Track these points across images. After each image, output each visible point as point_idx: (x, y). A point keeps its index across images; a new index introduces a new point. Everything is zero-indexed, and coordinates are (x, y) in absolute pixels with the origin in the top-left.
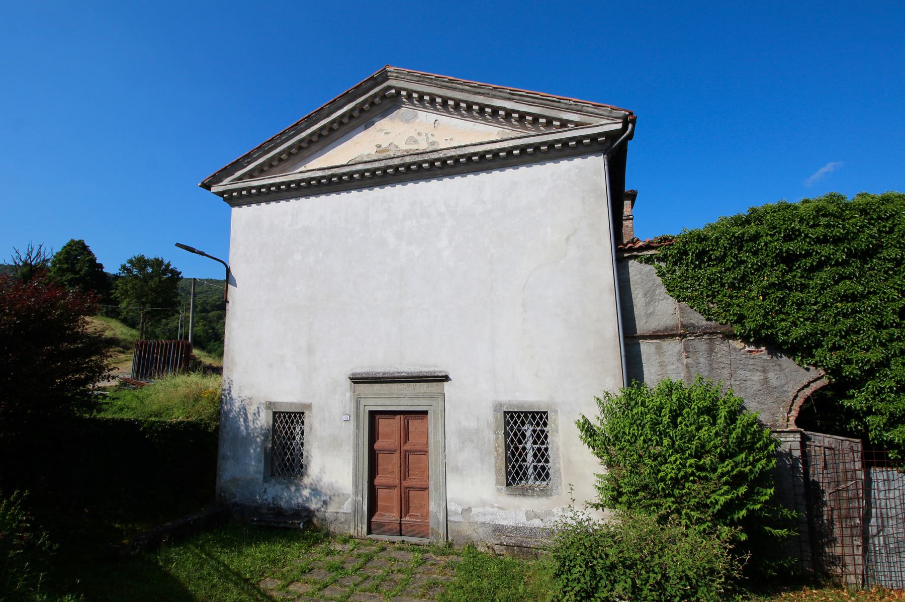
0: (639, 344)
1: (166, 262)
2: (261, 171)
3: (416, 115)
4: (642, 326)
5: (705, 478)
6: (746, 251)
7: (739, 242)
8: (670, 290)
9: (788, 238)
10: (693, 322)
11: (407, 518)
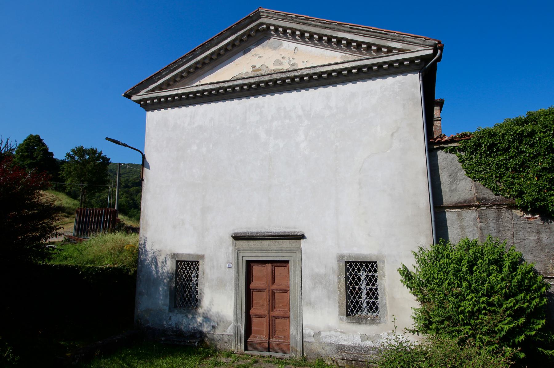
0: (445, 212)
1: (99, 151)
2: (167, 85)
4: (447, 199)
5: (494, 311)
7: (519, 137)
10: (485, 196)
11: (274, 339)
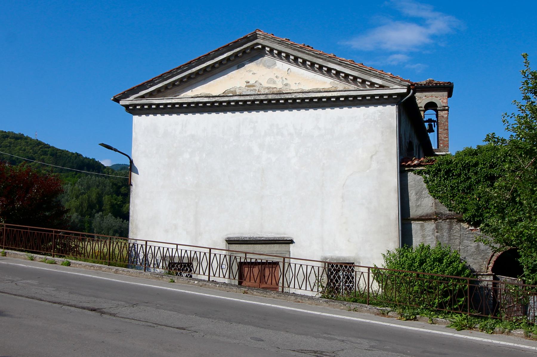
0: (411, 224)
3: (275, 64)
4: (413, 212)
5: (432, 292)
6: (472, 172)
7: (467, 167)
8: (431, 192)
9: (491, 167)
10: (442, 211)
